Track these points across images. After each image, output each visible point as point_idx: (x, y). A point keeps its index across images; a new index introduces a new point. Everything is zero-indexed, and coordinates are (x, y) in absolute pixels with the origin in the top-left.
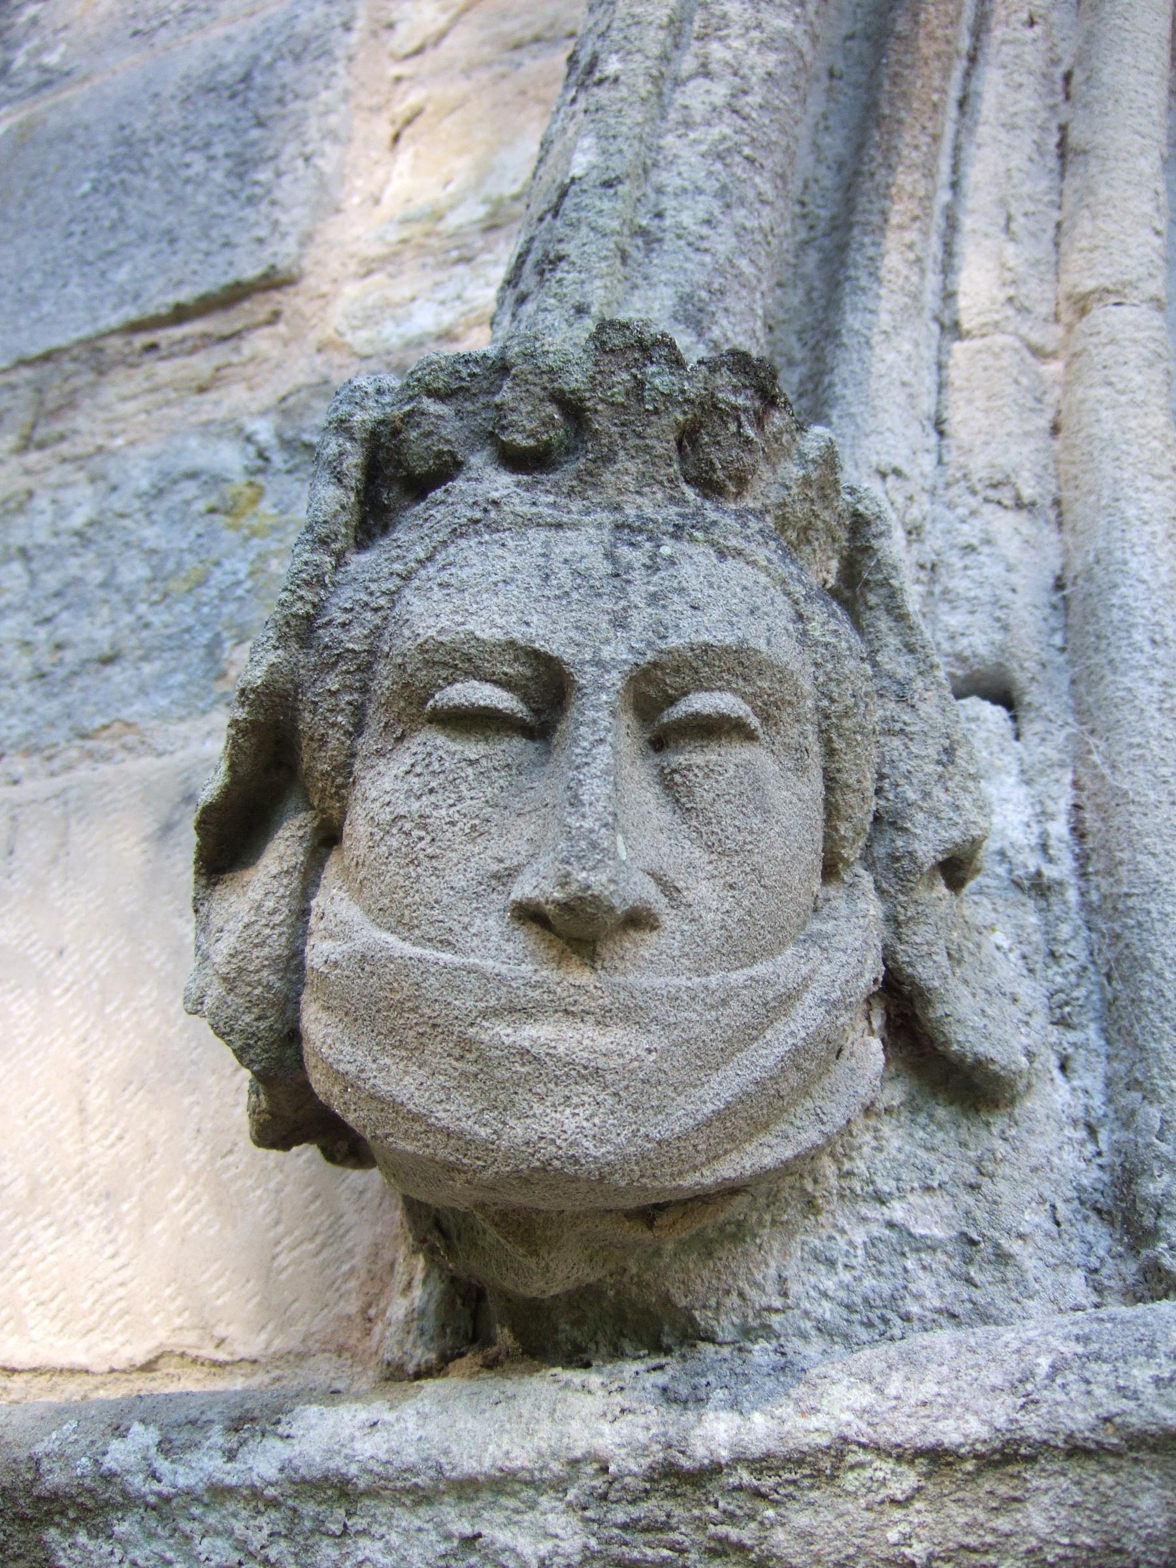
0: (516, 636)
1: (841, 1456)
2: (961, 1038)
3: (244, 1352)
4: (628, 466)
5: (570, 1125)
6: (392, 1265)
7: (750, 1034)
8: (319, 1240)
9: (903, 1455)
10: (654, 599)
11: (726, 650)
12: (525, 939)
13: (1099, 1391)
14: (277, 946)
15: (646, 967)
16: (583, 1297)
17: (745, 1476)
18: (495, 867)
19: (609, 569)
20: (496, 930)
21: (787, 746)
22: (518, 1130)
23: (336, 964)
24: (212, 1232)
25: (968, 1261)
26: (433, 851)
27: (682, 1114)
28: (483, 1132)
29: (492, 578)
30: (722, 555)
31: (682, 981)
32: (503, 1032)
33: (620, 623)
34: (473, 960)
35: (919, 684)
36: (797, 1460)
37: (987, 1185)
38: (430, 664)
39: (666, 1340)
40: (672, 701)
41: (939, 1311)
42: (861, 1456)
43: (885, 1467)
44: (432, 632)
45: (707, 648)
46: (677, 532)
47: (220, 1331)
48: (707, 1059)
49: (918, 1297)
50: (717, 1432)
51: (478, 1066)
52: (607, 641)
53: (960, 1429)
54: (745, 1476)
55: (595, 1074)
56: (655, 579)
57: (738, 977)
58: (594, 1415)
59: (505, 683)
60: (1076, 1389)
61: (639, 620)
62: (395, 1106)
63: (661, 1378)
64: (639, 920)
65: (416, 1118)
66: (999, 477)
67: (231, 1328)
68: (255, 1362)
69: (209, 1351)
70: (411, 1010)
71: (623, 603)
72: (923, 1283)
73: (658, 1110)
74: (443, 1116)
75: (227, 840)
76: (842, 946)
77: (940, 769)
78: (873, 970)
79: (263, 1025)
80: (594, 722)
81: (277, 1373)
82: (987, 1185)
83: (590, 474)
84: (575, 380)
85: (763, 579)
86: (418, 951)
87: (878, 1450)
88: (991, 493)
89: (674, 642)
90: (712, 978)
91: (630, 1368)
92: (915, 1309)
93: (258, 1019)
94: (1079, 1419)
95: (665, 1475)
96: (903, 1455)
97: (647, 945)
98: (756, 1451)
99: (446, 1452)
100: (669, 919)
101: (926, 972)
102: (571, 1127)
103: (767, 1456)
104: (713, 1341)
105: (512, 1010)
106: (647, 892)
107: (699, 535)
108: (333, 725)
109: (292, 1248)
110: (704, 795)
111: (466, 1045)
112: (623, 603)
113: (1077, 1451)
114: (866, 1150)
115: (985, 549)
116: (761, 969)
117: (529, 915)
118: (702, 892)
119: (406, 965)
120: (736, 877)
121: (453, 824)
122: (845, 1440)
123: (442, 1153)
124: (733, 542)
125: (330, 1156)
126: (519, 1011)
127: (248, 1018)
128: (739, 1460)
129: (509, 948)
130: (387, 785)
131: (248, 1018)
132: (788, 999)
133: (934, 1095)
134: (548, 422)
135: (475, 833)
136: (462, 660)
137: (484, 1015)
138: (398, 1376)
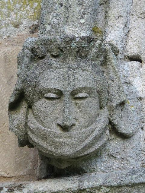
0: (56, 87)
1: (100, 187)
2: (121, 130)
3: (12, 175)
4: (69, 58)
5: (65, 150)
6: (37, 160)
7: (86, 138)
8: (24, 156)
9: (108, 187)
10: (74, 80)
11: (83, 88)
12: (59, 128)
13: (129, 179)
14: (24, 123)
15: (74, 131)
16: (68, 168)
17: (89, 190)
18: (55, 118)
19: (67, 76)
20: (55, 126)
21: (93, 96)
22: (59, 151)
23: (34, 128)
24: (3, 155)
25: (122, 161)
26: (46, 117)
27: (79, 148)
28: (55, 151)
29: (52, 78)
30: (83, 70)
31: (79, 132)
32: (56, 139)
33: (69, 84)
34: (52, 130)
35: (115, 77)
36: (96, 188)
37: (125, 150)
38: (44, 90)
39: (80, 173)
40: (76, 94)
41: (118, 168)
42: (103, 187)
43: (105, 188)
44: (44, 87)
45: (80, 88)
46: (77, 68)
47: (8, 172)
48: (82, 141)
49: (115, 166)
50: (86, 184)
51: (54, 144)
52: (67, 88)
53: (114, 184)
54: (89, 190)
55: (68, 144)
56: (74, 77)
57: (86, 130)
58: (70, 183)
59: (55, 93)
60: (127, 179)
61: (72, 84)
62: (43, 147)
63: (79, 178)
64: (74, 125)
65: (46, 149)
66: (141, 12)
67: (10, 172)
68: (15, 177)
69: (7, 175)
70: (45, 136)
71: (69, 81)
72: (116, 164)
73: (76, 148)
74: (49, 149)
75: (13, 106)
76: (102, 121)
77: (117, 92)
78: (109, 122)
79: (22, 134)
80: (66, 100)
81: (19, 178)
82: (125, 150)
83: (64, 59)
84: (62, 46)
85: (89, 73)
86: (45, 128)
87: (105, 186)
88: (140, 16)
89: (76, 87)
90: (82, 131)
91: (75, 177)
92: (114, 168)
93: (22, 133)
94: (127, 182)
95: (79, 190)
96: (108, 187)
97: (74, 128)
98: (90, 187)
99: (51, 189)
100: (77, 124)
101: (115, 122)
102: (66, 151)
103: (92, 187)
104: (87, 173)
105: (58, 137)
106: (73, 121)
107: (80, 68)
108: (30, 94)
109: (19, 157)
110: (81, 107)
111: (52, 141)
112: (69, 81)
113: (127, 186)
114: (108, 146)
115: (138, 29)
116: (89, 128)
117: (59, 125)
118: (81, 120)
119: (44, 130)
120: (85, 117)
121: (49, 112)
122: (101, 185)
123: (50, 153)
124: (85, 68)
125: (29, 147)
126: (59, 137)
127: (20, 133)
128: (88, 188)
129: (57, 129)
130: (40, 104)
131: (20, 133)
132: (93, 132)
133: (118, 137)
134: (58, 52)
135: (52, 113)
136: (49, 91)
137: (54, 137)
138: (39, 179)
